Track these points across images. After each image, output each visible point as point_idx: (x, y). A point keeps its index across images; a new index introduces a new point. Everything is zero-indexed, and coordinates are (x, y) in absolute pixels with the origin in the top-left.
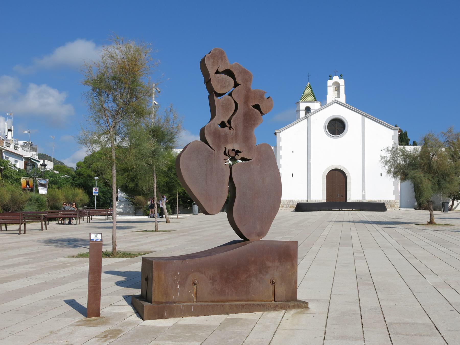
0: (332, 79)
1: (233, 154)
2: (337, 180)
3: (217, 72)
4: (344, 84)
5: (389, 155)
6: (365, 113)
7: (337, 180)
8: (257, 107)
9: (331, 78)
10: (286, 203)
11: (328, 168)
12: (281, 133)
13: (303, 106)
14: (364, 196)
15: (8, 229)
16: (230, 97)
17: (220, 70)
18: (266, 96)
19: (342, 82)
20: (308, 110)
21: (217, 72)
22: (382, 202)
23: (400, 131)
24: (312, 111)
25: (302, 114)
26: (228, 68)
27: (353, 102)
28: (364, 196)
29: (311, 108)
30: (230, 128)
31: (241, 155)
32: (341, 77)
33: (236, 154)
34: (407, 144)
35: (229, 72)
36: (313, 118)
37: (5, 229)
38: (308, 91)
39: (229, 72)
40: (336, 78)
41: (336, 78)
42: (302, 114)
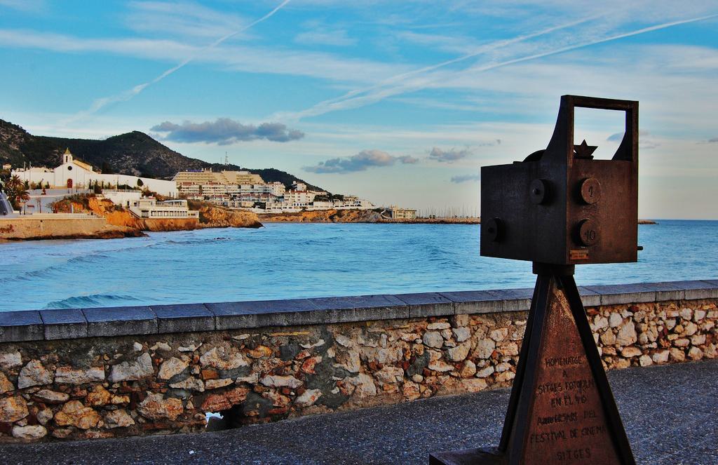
13: (65, 156)
14: (646, 134)
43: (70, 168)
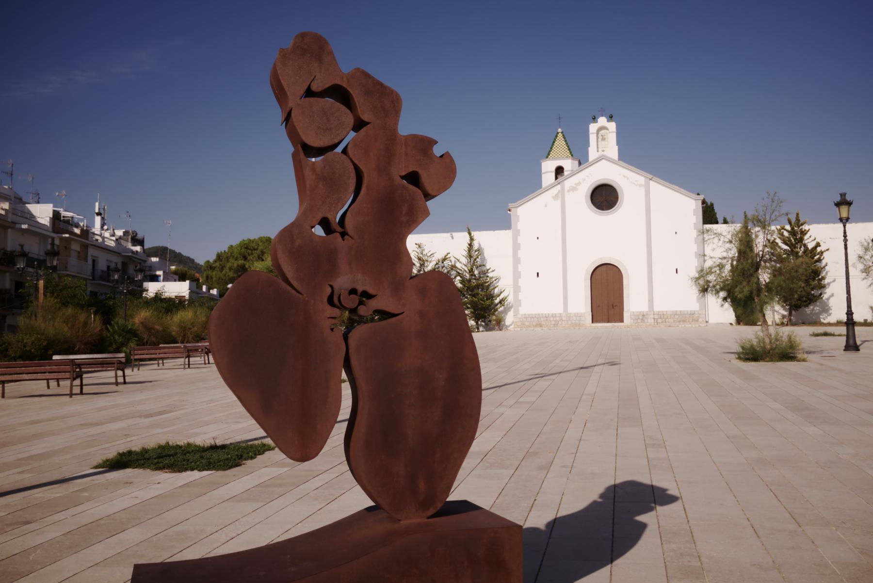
1: (351, 302)
3: (309, 93)
4: (615, 130)
5: (769, 347)
6: (650, 176)
7: (607, 289)
8: (413, 178)
9: (594, 119)
10: (529, 319)
12: (519, 209)
13: (548, 167)
15: (84, 391)
16: (344, 156)
17: (315, 87)
18: (438, 151)
19: (612, 126)
20: (559, 171)
21: (309, 93)
22: (621, 163)
23: (704, 202)
24: (566, 173)
25: (548, 177)
26: (338, 82)
27: (629, 155)
29: (565, 169)
30: (344, 234)
31: (374, 304)
32: (611, 118)
33: (361, 303)
34: (717, 223)
35: (339, 94)
36: (569, 183)
37: (79, 392)
39: (339, 94)
40: (602, 121)
41: (602, 121)
42: (548, 177)
43: (604, 197)
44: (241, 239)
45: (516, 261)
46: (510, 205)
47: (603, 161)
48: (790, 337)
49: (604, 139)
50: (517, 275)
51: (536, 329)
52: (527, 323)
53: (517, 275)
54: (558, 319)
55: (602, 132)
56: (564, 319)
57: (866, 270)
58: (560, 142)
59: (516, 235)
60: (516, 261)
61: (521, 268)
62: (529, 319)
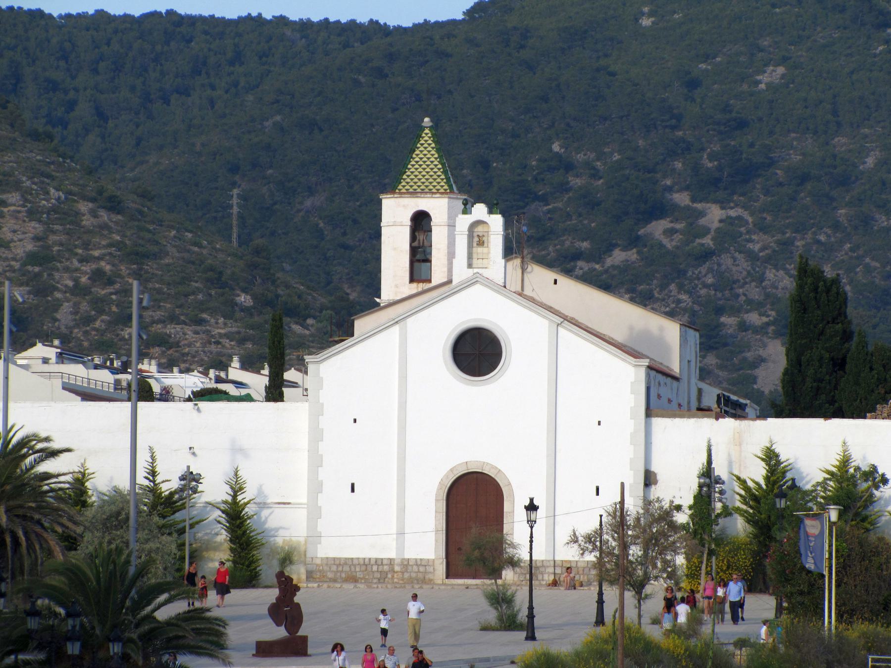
0: (491, 212)
2: (473, 503)
7: (473, 503)
11: (451, 470)
13: (396, 212)
14: (401, 547)
28: (401, 547)
38: (426, 155)
43: (477, 352)
44: (85, 11)
45: (316, 461)
46: (308, 358)
47: (477, 287)
48: (771, 457)
49: (481, 243)
50: (316, 488)
51: (346, 586)
52: (330, 575)
53: (316, 488)
54: (386, 568)
55: (480, 229)
56: (397, 568)
57: (888, 2)
58: (426, 155)
59: (317, 413)
60: (316, 461)
61: (322, 474)
62: (334, 568)
